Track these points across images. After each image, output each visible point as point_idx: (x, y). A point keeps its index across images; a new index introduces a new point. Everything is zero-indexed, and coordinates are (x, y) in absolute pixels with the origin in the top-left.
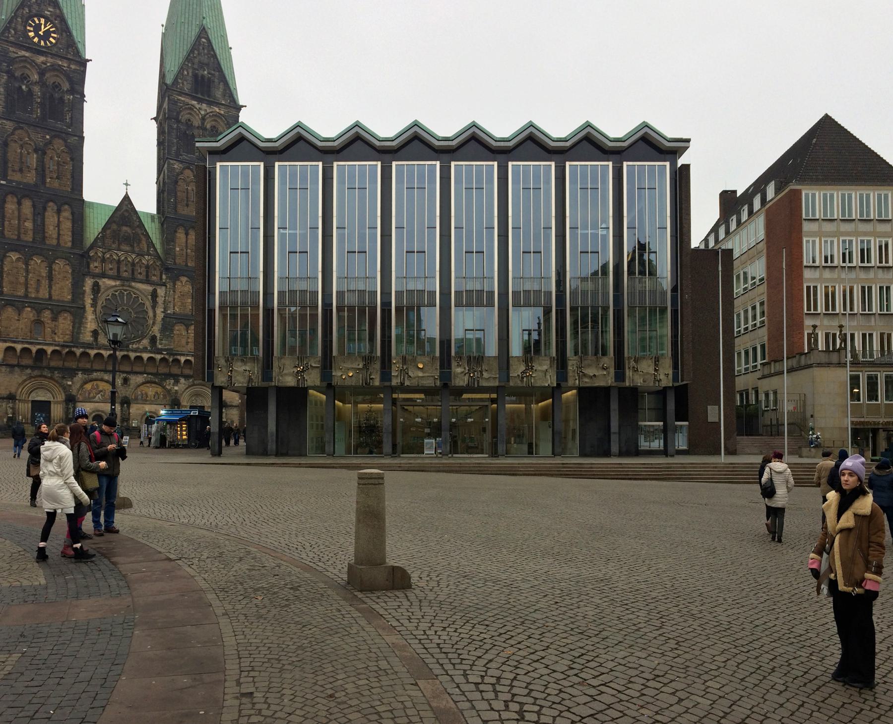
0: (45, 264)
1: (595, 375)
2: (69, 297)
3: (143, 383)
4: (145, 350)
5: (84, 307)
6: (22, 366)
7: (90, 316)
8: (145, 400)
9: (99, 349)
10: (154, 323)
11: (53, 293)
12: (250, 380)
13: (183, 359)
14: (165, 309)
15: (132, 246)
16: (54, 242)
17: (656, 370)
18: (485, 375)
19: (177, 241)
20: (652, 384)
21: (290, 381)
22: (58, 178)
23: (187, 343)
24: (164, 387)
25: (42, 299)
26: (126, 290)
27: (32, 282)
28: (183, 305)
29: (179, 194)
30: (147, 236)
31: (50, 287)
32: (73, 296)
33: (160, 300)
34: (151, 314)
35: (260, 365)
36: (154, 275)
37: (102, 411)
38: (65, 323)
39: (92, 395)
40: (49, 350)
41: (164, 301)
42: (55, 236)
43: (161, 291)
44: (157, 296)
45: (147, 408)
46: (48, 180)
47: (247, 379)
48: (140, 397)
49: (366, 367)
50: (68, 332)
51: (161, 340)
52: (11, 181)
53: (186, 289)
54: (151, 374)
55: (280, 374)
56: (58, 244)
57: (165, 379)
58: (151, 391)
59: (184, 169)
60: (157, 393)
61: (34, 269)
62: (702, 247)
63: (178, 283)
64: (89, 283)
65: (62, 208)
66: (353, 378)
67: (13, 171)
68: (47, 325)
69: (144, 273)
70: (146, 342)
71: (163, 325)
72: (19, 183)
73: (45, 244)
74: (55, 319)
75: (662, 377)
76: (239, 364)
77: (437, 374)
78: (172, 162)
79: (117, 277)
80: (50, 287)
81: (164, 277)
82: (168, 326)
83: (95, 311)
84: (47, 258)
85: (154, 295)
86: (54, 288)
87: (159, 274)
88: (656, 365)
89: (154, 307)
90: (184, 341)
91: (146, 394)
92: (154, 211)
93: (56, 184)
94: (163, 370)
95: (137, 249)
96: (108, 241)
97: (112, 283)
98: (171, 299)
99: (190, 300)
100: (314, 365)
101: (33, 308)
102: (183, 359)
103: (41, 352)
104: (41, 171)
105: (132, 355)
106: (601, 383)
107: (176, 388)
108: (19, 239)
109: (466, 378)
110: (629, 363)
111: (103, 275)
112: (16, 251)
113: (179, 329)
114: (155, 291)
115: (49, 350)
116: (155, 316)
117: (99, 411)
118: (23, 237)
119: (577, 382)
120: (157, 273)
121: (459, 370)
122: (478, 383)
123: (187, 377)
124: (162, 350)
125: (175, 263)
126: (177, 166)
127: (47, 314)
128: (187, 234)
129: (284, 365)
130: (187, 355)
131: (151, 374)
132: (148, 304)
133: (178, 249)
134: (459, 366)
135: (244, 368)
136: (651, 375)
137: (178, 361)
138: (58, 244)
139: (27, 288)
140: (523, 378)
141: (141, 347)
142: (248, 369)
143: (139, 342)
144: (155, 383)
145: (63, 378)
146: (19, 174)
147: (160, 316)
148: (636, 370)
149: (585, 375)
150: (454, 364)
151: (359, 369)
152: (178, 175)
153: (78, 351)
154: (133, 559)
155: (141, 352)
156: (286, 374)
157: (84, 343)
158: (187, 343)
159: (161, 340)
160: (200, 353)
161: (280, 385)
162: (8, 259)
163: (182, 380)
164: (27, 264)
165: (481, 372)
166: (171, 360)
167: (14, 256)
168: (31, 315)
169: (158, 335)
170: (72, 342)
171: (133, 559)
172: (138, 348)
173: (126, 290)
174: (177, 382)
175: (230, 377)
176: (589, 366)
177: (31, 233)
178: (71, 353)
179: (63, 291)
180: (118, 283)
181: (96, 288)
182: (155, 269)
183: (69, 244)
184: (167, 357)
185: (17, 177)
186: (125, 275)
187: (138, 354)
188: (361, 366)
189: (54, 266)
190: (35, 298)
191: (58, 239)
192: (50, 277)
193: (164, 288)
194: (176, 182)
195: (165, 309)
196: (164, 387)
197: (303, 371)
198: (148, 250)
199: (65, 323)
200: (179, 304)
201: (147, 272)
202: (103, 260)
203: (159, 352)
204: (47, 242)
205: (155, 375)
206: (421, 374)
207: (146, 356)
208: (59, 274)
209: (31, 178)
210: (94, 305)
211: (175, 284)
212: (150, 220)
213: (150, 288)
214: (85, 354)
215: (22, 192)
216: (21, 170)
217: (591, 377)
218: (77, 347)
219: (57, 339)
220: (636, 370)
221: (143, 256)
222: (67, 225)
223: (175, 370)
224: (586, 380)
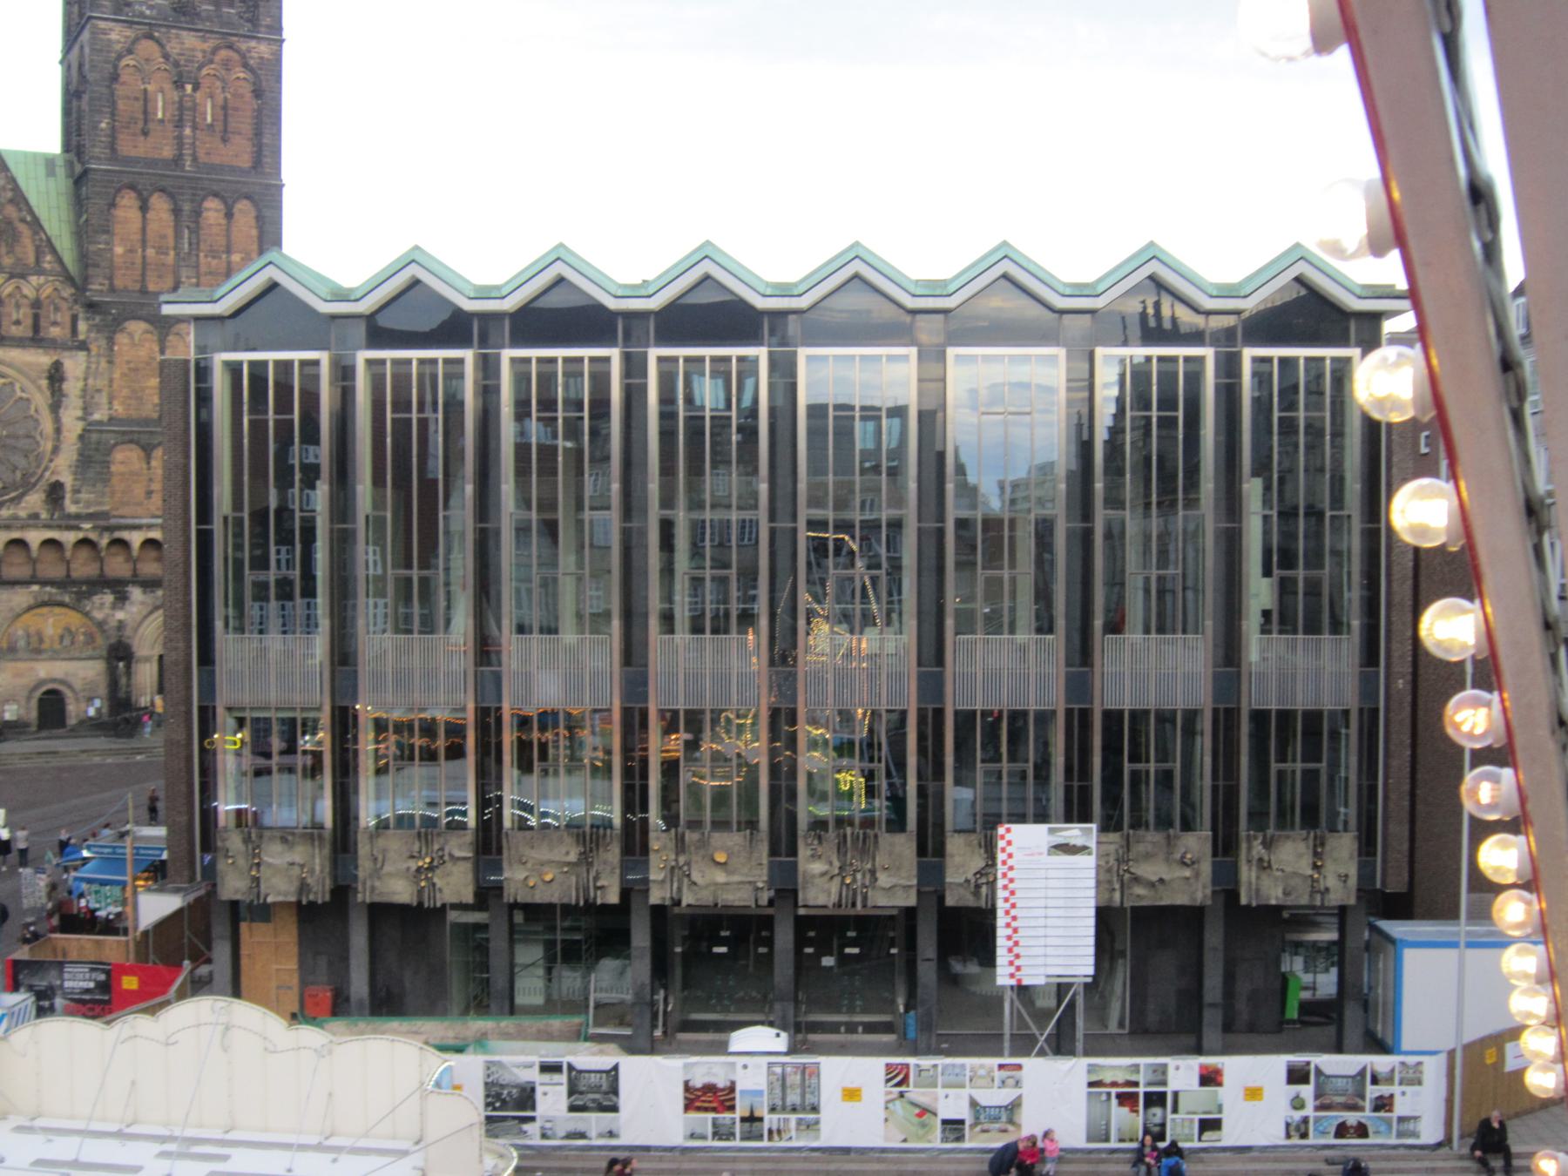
1: (1161, 880)
3: (30, 608)
10: (56, 450)
12: (303, 887)
13: (136, 539)
14: (85, 409)
17: (1315, 867)
18: (884, 880)
19: (118, 229)
20: (1304, 901)
21: (400, 891)
23: (149, 493)
24: (87, 614)
29: (121, 105)
30: (36, 224)
33: (72, 387)
34: (47, 425)
35: (327, 851)
36: (55, 323)
41: (84, 390)
43: (75, 365)
44: (62, 379)
47: (296, 884)
48: (22, 643)
49: (585, 860)
51: (76, 491)
53: (142, 353)
54: (52, 583)
55: (376, 873)
57: (89, 595)
58: (51, 623)
59: (136, 40)
63: (122, 339)
66: (554, 886)
69: (29, 322)
70: (34, 500)
71: (81, 454)
75: (1331, 881)
76: (277, 847)
77: (761, 877)
78: (102, 25)
81: (82, 326)
82: (93, 459)
85: (56, 376)
87: (67, 319)
88: (1316, 854)
89: (55, 407)
90: (139, 490)
92: (51, 142)
94: (83, 567)
98: (101, 383)
99: (154, 382)
100: (458, 854)
102: (136, 539)
106: (1181, 899)
107: (120, 615)
109: (834, 887)
110: (1249, 849)
113: (126, 458)
114: (57, 366)
116: (58, 431)
119: (1117, 896)
120: (64, 317)
121: (817, 867)
122: (865, 898)
123: (149, 584)
124: (78, 517)
125: (112, 289)
126: (117, 35)
128: (144, 208)
129: (384, 851)
130: (150, 527)
131: (52, 583)
132: (40, 400)
133: (119, 250)
134: (815, 857)
135: (289, 858)
136: (1305, 877)
137: (123, 544)
140: (978, 887)
141: (23, 514)
142: (298, 858)
143: (17, 500)
144: (61, 604)
147: (72, 424)
148: (1264, 866)
149: (1137, 880)
150: (803, 852)
151: (568, 864)
152: (120, 57)
155: (22, 528)
156: (390, 875)
158: (149, 493)
159: (76, 491)
160: (183, 819)
161: (377, 899)
163: (136, 593)
165: (873, 872)
166: (104, 541)
175: (257, 880)
176: (1148, 856)
182: (57, 309)
184: (93, 536)
187: (16, 535)
188: (573, 857)
193: (82, 355)
194: (115, 77)
196: (87, 614)
197: (431, 868)
198: (38, 260)
203: (71, 522)
205: (64, 583)
206: (721, 877)
207: (34, 537)
211: (111, 341)
212: (42, 171)
217: (1152, 885)
220: (1264, 866)
223: (117, 566)
224: (1139, 890)
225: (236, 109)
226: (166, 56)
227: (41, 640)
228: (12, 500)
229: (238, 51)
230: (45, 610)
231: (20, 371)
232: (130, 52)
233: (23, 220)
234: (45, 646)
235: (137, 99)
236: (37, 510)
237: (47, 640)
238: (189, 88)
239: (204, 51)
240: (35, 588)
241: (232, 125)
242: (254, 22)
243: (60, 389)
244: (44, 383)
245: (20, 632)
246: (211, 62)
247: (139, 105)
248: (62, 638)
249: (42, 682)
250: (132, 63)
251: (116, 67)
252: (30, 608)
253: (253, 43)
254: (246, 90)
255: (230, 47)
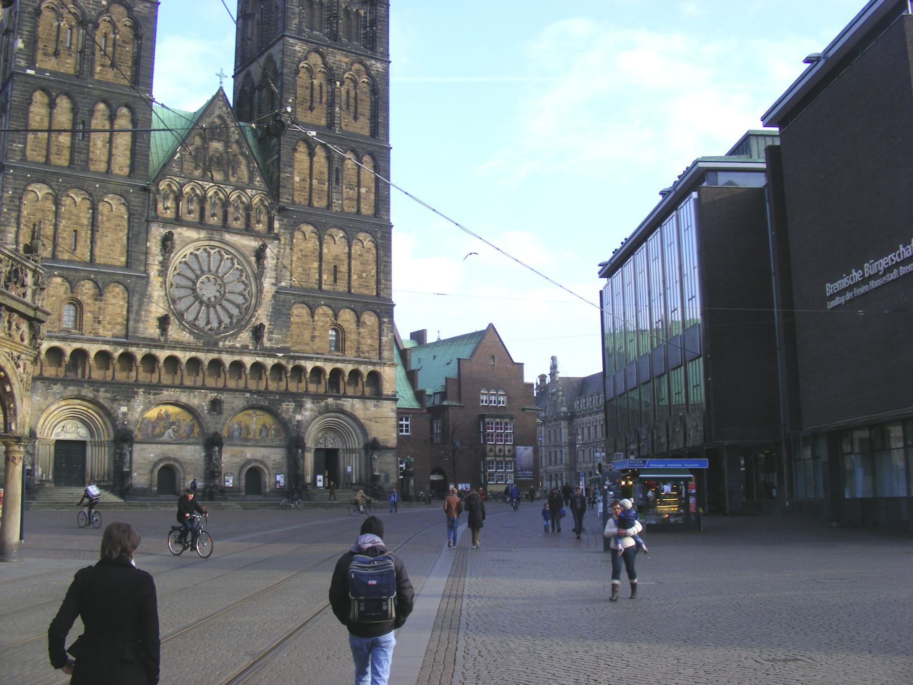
0: (88, 204)
2: (123, 259)
3: (244, 409)
4: (244, 350)
5: (148, 277)
6: (47, 379)
7: (156, 291)
8: (245, 439)
9: (174, 348)
11: (97, 252)
15: (226, 175)
16: (102, 167)
19: (296, 165)
22: (113, 65)
25: (79, 263)
26: (213, 247)
27: (65, 235)
28: (306, 272)
31: (93, 242)
32: (128, 257)
33: (270, 262)
37: (176, 460)
38: (116, 300)
39: (157, 430)
40: (93, 349)
42: (105, 158)
45: (250, 453)
46: (98, 69)
48: (236, 434)
50: (120, 320)
51: (271, 333)
52: (41, 71)
56: (109, 170)
60: (264, 426)
61: (70, 212)
62: (870, 496)
63: (298, 235)
64: (157, 232)
65: (118, 113)
67: (45, 54)
68: (86, 308)
69: (220, 215)
70: (245, 337)
72: (54, 73)
73: (88, 171)
74: (99, 295)
78: (291, 41)
79: (201, 224)
80: (93, 242)
81: (276, 225)
83: (165, 282)
84: (90, 195)
85: (260, 254)
86: (99, 243)
91: (247, 427)
93: (110, 75)
95: (232, 179)
96: (188, 165)
97: (192, 234)
101: (66, 279)
103: (80, 355)
104: (86, 55)
105: (227, 359)
107: (298, 417)
108: (47, 162)
111: (178, 221)
112: (43, 182)
115: (93, 349)
117: (169, 459)
118: (54, 159)
127: (87, 289)
130: (317, 359)
133: (297, 179)
138: (109, 170)
139: (55, 246)
145: (114, 400)
146: (53, 59)
152: (300, 61)
153: (139, 353)
154: (849, 296)
157: (145, 339)
159: (271, 333)
162: (31, 196)
164: (57, 203)
166: (290, 367)
167: (41, 190)
168: (63, 289)
169: (266, 324)
170: (127, 337)
171: (849, 296)
172: (233, 347)
173: (213, 247)
174: (300, 406)
177: (66, 153)
178: (127, 358)
179: (112, 249)
180: (203, 234)
181: (167, 243)
183: (126, 171)
184: (283, 362)
185: (50, 64)
186: (215, 221)
189: (100, 207)
190: (69, 262)
191: (109, 162)
192: (94, 225)
194: (297, 72)
195: (278, 279)
199: (116, 300)
200: (300, 270)
201: (248, 217)
202: (178, 198)
203: (270, 353)
204: (92, 168)
207: (248, 361)
208: (109, 220)
209: (68, 65)
210: (163, 273)
211: (292, 237)
213: (255, 244)
214: (150, 360)
215: (54, 86)
216: (56, 54)
218: (137, 345)
219: (101, 331)
221: (243, 189)
222: (123, 141)
225: (362, 100)
226: (325, 63)
227: (248, 433)
228: (232, 335)
229: (364, 65)
230: (250, 412)
231: (238, 251)
232: (306, 59)
233: (243, 154)
234: (250, 437)
235: (307, 88)
236: (247, 343)
237: (252, 433)
238: (338, 83)
239: (346, 63)
240: (248, 395)
241: (359, 110)
242: (373, 49)
243: (263, 264)
244: (253, 259)
245: (236, 426)
246: (351, 70)
247: (309, 91)
248: (261, 431)
249: (248, 462)
250: (306, 66)
251: (298, 66)
252: (244, 409)
253: (373, 62)
254: (366, 89)
255: (361, 63)
